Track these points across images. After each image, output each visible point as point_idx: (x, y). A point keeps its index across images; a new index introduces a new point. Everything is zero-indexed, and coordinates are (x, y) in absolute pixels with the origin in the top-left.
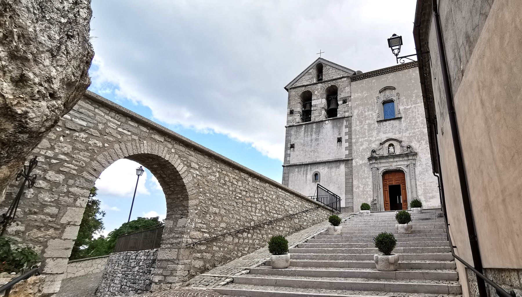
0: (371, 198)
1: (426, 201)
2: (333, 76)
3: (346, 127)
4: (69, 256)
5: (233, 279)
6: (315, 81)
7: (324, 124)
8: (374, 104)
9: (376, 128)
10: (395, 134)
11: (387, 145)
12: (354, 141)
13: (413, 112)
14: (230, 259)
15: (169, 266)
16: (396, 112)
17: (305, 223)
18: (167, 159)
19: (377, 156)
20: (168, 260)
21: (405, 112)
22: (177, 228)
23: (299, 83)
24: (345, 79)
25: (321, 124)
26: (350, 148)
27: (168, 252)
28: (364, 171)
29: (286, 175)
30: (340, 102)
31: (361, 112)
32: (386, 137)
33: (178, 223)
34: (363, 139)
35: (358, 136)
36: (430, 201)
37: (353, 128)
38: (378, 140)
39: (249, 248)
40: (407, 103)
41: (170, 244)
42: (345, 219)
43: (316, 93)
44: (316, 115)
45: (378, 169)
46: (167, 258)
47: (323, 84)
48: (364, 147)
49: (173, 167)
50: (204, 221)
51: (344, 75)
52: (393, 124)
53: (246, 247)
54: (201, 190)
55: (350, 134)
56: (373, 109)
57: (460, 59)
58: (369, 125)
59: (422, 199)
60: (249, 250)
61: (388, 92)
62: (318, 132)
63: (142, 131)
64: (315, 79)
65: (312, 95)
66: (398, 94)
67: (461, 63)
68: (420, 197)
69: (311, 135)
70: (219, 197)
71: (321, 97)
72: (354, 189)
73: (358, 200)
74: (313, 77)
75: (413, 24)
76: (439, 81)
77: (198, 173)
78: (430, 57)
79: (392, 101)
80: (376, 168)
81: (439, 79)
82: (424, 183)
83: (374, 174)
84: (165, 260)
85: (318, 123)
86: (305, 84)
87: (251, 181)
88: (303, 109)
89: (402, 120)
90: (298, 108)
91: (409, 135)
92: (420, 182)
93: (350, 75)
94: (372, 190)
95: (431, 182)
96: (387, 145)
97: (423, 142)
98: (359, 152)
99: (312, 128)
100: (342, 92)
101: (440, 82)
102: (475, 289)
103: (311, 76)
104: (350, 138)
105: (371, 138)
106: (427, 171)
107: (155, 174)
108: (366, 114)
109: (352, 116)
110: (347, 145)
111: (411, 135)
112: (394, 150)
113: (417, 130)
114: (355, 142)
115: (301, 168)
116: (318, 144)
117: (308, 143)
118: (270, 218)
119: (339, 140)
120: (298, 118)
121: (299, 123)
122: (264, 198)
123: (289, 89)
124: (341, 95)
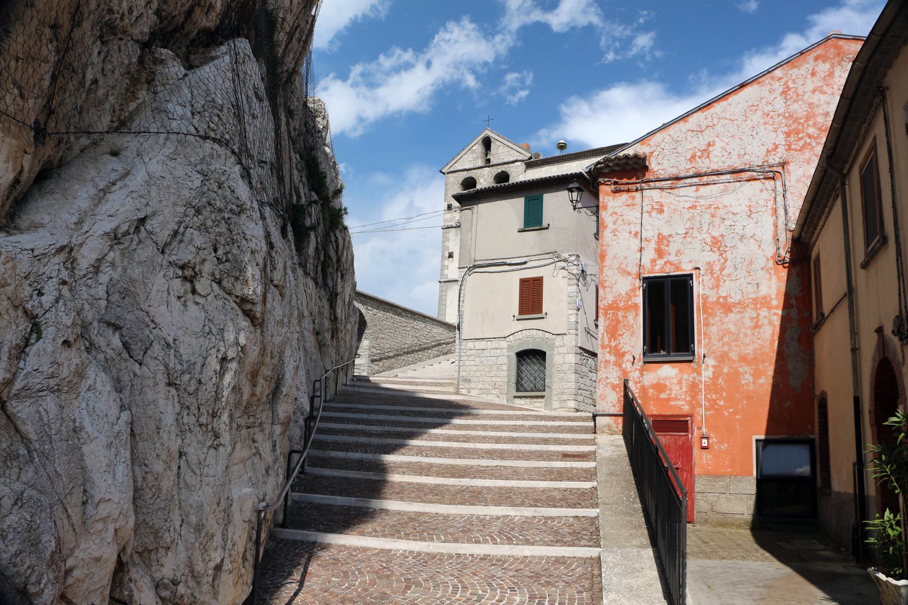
4: (339, 297)
6: (480, 163)
14: (393, 368)
24: (519, 163)
74: (478, 157)
86: (467, 167)
103: (475, 155)
114: (615, 355)
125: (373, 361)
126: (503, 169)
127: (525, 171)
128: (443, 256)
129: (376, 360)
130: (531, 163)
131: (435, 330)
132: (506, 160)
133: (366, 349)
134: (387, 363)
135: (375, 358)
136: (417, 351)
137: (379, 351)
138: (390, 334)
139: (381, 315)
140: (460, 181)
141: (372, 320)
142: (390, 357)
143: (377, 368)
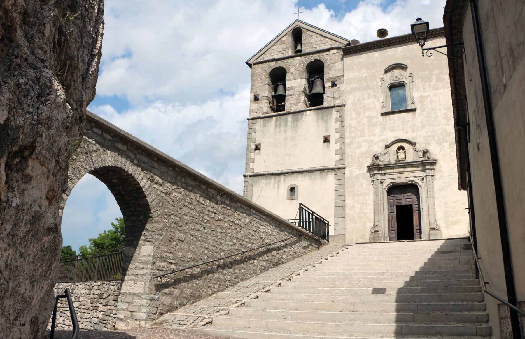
0: (370, 222)
1: (447, 228)
2: (317, 46)
3: (337, 120)
5: (212, 319)
6: (290, 53)
7: (304, 116)
8: (377, 88)
9: (380, 123)
10: (407, 132)
11: (395, 147)
12: (347, 141)
13: (432, 101)
14: (200, 298)
15: (135, 301)
16: (409, 101)
17: (284, 256)
18: (130, 173)
19: (380, 163)
20: (134, 294)
21: (421, 101)
22: (141, 257)
23: (267, 55)
24: (335, 51)
25: (300, 115)
26: (342, 152)
27: (133, 285)
28: (362, 184)
29: (249, 189)
30: (328, 85)
31: (359, 100)
32: (395, 137)
33: (141, 251)
34: (360, 139)
35: (353, 135)
36: (452, 228)
37: (346, 123)
38: (383, 140)
39: (220, 285)
40: (424, 89)
41: (133, 275)
42: (337, 252)
43: (292, 70)
44: (292, 102)
45: (381, 183)
46: (132, 292)
47: (303, 57)
48: (363, 150)
49: (136, 183)
50: (170, 250)
51: (333, 46)
52: (404, 119)
53: (216, 284)
54: (166, 210)
55: (341, 130)
56: (375, 96)
57: (503, 71)
58: (370, 118)
59: (441, 223)
60: (219, 287)
61: (397, 72)
62: (295, 127)
63: (106, 139)
64: (290, 51)
65: (286, 73)
66: (411, 76)
67: (503, 75)
68: (438, 222)
69: (285, 131)
70: (185, 219)
71: (299, 75)
72: (347, 211)
73: (353, 225)
74: (288, 47)
75: (444, 9)
76: (475, 85)
77: (162, 189)
78: (465, 51)
79: (402, 85)
80: (379, 181)
81: (475, 83)
82: (446, 203)
83: (377, 190)
84: (130, 294)
85: (295, 114)
86: (276, 57)
87: (220, 200)
88: (273, 93)
89: (417, 112)
90: (266, 92)
91: (427, 133)
92: (440, 201)
93: (341, 45)
94: (372, 212)
95: (455, 202)
96: (395, 147)
97: (446, 145)
98: (355, 158)
99: (286, 121)
100: (330, 69)
101: (477, 87)
102: (508, 326)
103: (284, 46)
104: (343, 137)
105: (372, 138)
106: (450, 186)
107: (112, 191)
108: (366, 101)
109: (344, 106)
110: (338, 146)
111: (429, 134)
112: (405, 155)
113: (438, 127)
115: (271, 179)
116: (295, 145)
117: (280, 143)
118: (242, 247)
119: (326, 140)
120: (265, 106)
121: (267, 113)
122: (235, 222)
123: (252, 64)
124: (329, 74)
125: (159, 287)
126: (316, 58)
127: (342, 59)
128: (248, 148)
129: (166, 286)
130: (349, 49)
131: (263, 229)
132: (319, 48)
133: (146, 263)
134: (187, 288)
135: (165, 280)
136: (238, 262)
137: (173, 267)
138: (196, 233)
139: (179, 196)
140: (268, 72)
141: (161, 203)
142: (193, 277)
143: (167, 300)
